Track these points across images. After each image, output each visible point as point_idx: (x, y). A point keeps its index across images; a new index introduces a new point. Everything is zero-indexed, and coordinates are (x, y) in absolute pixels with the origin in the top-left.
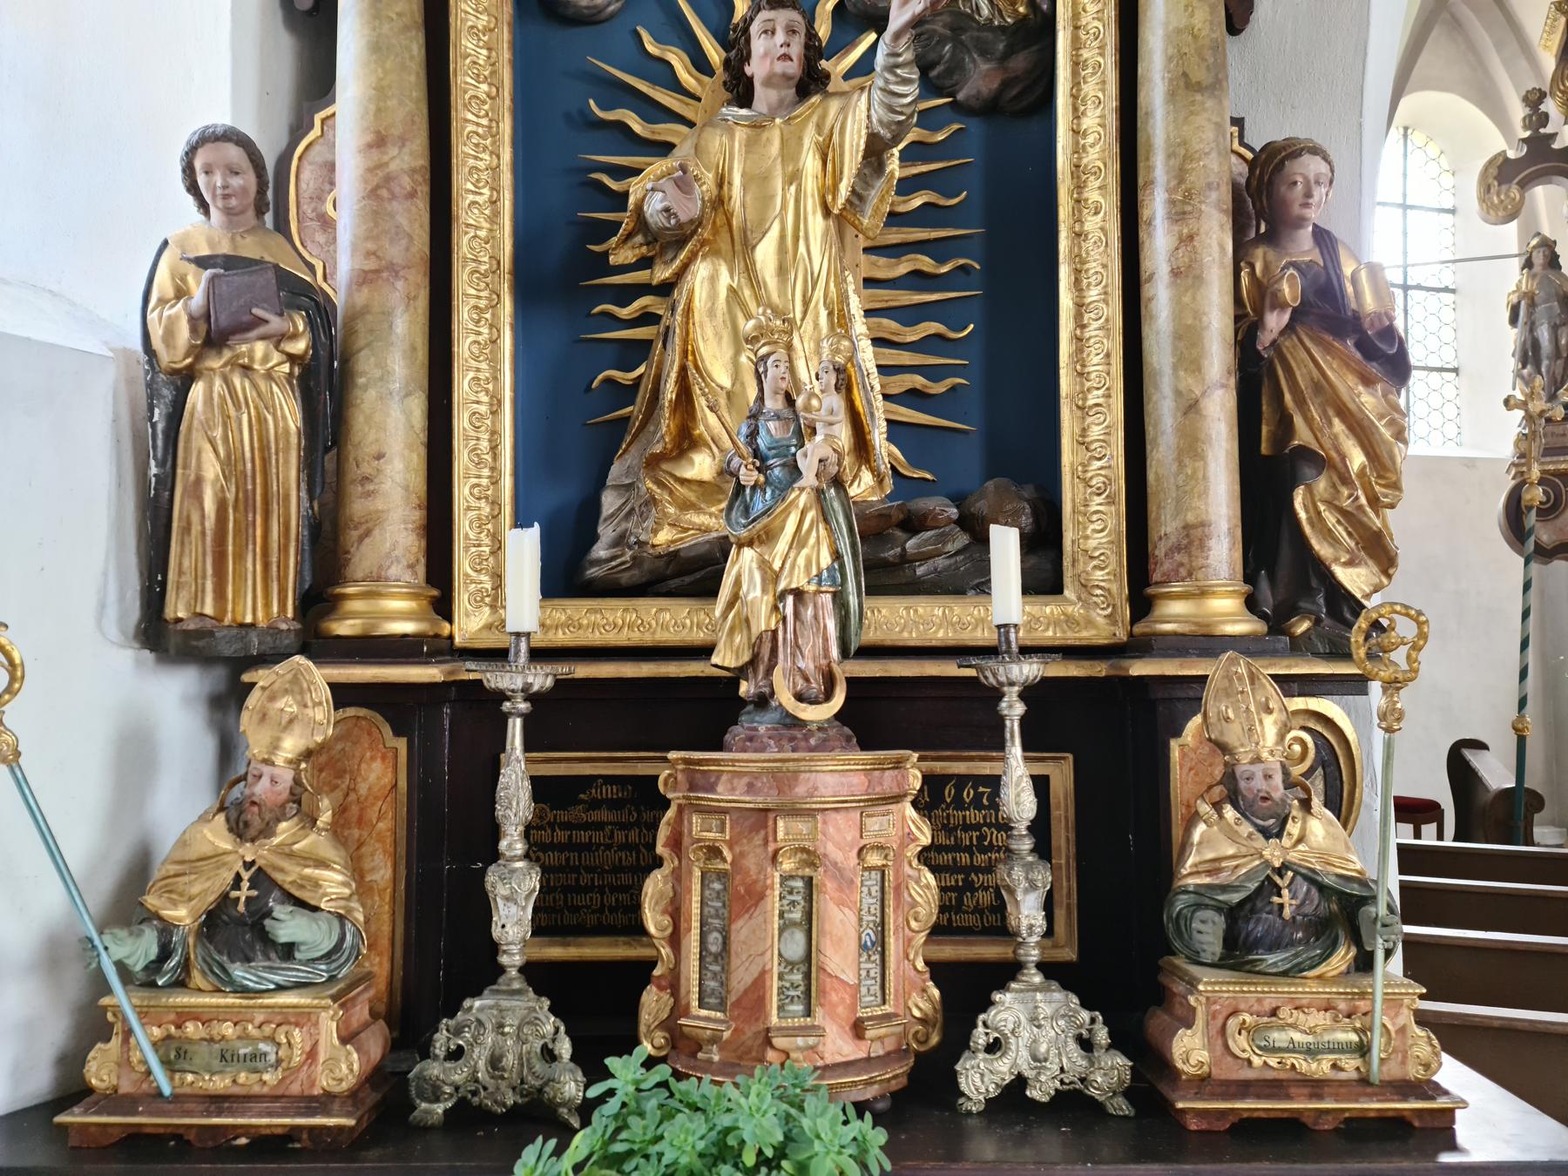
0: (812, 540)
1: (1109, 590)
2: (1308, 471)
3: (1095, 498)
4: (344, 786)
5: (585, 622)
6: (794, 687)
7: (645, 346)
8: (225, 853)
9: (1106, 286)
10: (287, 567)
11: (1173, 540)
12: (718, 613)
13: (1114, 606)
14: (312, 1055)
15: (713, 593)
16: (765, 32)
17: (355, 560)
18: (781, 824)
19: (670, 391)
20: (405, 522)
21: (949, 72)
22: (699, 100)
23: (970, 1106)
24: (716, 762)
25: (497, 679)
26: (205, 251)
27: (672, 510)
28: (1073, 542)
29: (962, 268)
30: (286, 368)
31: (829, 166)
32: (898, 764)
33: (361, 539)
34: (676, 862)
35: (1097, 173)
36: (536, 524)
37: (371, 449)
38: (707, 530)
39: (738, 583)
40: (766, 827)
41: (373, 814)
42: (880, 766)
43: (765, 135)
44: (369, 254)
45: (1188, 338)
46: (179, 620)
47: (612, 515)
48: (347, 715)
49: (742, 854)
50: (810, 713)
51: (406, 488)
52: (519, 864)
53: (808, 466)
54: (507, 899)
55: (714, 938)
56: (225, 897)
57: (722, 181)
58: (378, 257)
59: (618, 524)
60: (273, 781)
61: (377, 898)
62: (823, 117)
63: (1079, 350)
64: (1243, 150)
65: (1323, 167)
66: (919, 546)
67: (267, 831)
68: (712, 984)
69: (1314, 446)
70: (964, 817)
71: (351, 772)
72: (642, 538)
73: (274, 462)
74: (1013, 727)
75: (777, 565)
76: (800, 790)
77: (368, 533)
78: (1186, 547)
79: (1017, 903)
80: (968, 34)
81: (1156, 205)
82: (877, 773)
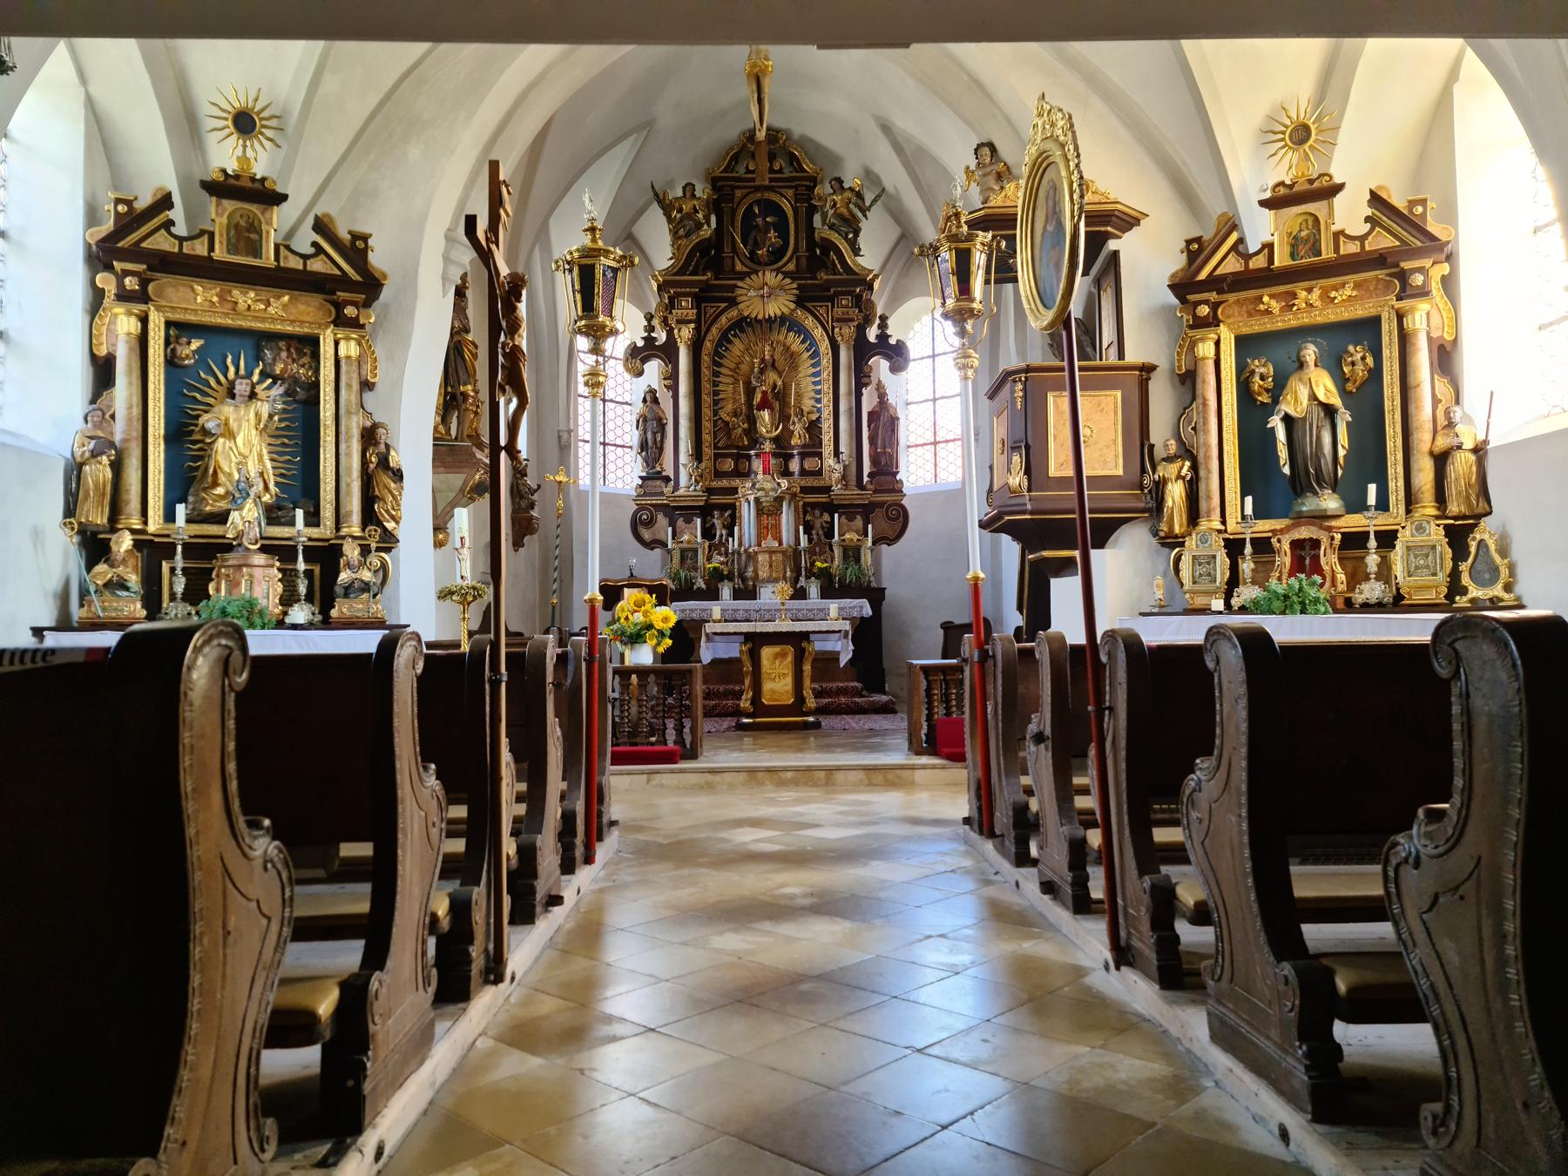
15: (226, 523)
19: (211, 471)
50: (251, 547)
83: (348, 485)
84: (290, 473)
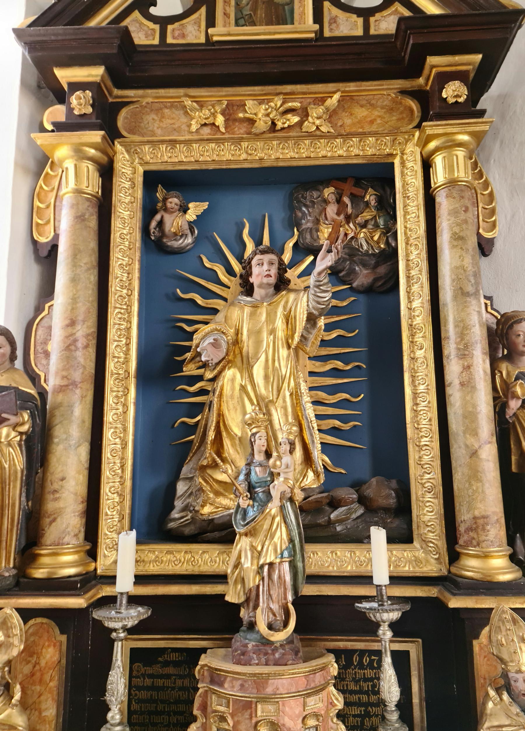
0: (278, 534)
1: (436, 545)
3: (428, 494)
4: (33, 661)
5: (165, 559)
6: (268, 619)
7: (202, 405)
9: (428, 385)
10: (11, 540)
11: (468, 524)
13: (440, 554)
16: (259, 264)
17: (47, 535)
18: (259, 706)
19: (211, 435)
20: (74, 512)
21: (348, 274)
22: (229, 288)
27: (211, 495)
28: (417, 516)
29: (358, 366)
30: (18, 438)
31: (290, 326)
34: (205, 720)
35: (420, 330)
36: (134, 530)
37: (60, 476)
39: (239, 557)
40: (251, 708)
41: (47, 677)
43: (259, 311)
44: (63, 377)
47: (182, 495)
48: (37, 622)
50: (279, 637)
51: (76, 494)
53: (275, 493)
57: (238, 332)
58: (68, 379)
59: (185, 500)
61: (47, 726)
62: (287, 302)
64: (493, 312)
70: (364, 673)
71: (37, 653)
72: (196, 508)
73: (7, 489)
77: (54, 520)
78: (475, 529)
80: (357, 258)
82: (312, 676)
83: (474, 454)
84: (346, 427)
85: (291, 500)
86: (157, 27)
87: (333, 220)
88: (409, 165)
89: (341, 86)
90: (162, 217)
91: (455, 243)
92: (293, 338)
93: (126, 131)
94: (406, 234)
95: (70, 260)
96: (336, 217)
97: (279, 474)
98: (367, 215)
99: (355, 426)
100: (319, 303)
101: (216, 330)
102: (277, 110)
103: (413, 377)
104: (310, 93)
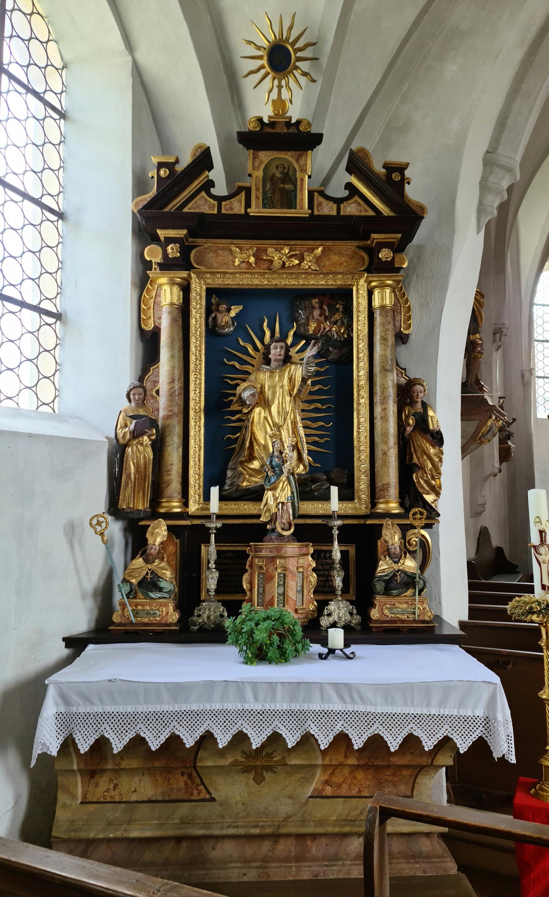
0: (286, 489)
2: (416, 469)
8: (143, 567)
12: (262, 508)
14: (167, 614)
18: (278, 561)
22: (255, 358)
23: (323, 628)
24: (262, 545)
25: (208, 525)
26: (131, 414)
27: (247, 477)
30: (150, 443)
32: (307, 546)
33: (167, 487)
38: (258, 483)
39: (267, 500)
42: (302, 546)
43: (274, 375)
44: (170, 411)
45: (385, 434)
46: (124, 509)
49: (268, 568)
50: (286, 533)
52: (214, 570)
53: (285, 470)
54: (211, 578)
55: (261, 589)
56: (144, 577)
60: (155, 549)
62: (290, 370)
63: (359, 435)
65: (422, 388)
66: (315, 487)
67: (154, 562)
68: (260, 600)
69: (418, 463)
72: (239, 484)
74: (336, 537)
75: (277, 496)
76: (283, 552)
77: (169, 485)
79: (335, 580)
81: (377, 399)
83: (385, 453)
84: (322, 441)
85: (293, 474)
86: (216, 203)
87: (317, 319)
88: (361, 292)
89: (324, 242)
90: (216, 315)
91: (382, 342)
92: (293, 391)
93: (195, 263)
94: (357, 333)
95: (170, 345)
96: (319, 317)
97: (287, 461)
98: (337, 317)
99: (327, 441)
100: (308, 372)
101: (251, 385)
102: (286, 255)
103: (358, 414)
104: (305, 245)
